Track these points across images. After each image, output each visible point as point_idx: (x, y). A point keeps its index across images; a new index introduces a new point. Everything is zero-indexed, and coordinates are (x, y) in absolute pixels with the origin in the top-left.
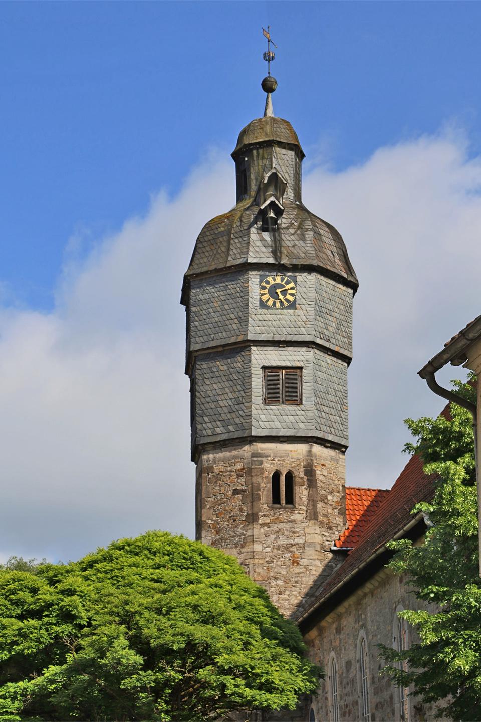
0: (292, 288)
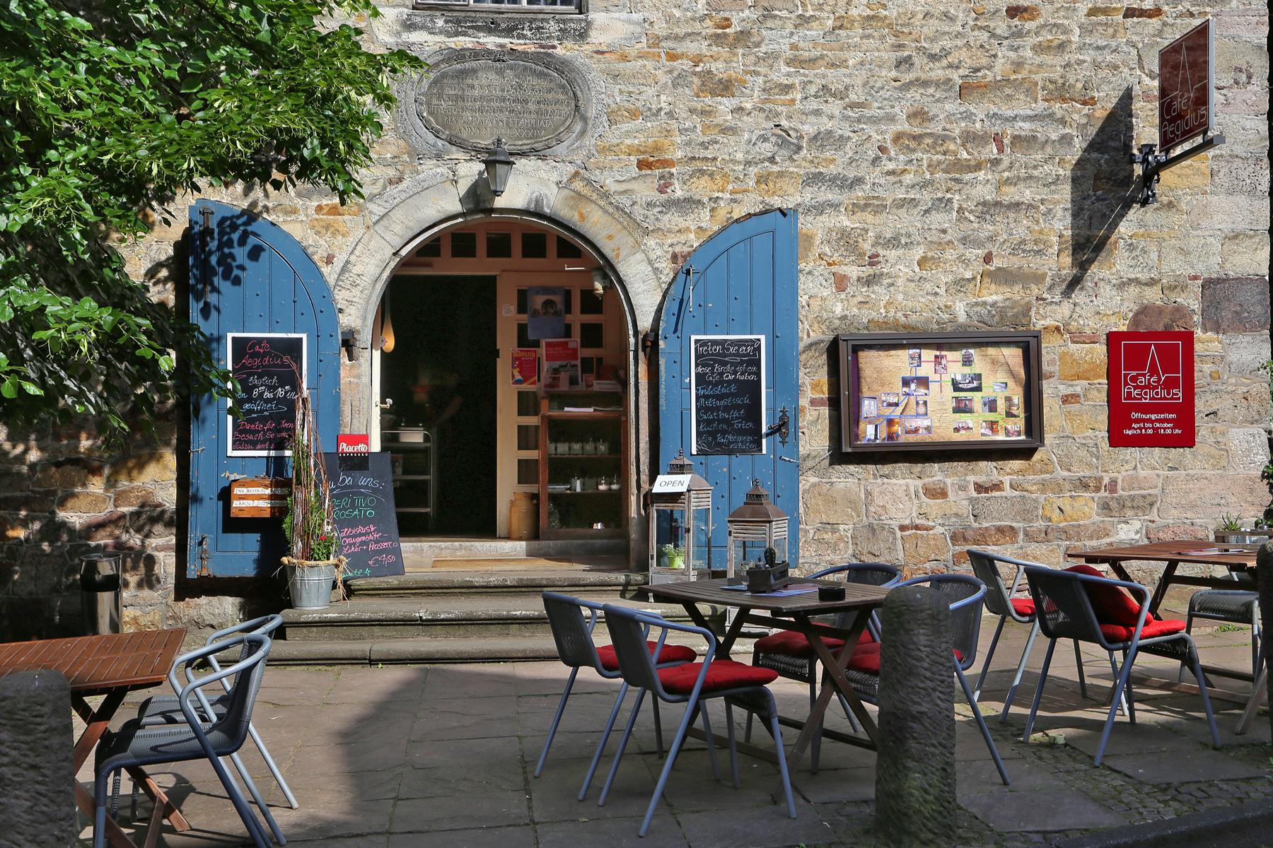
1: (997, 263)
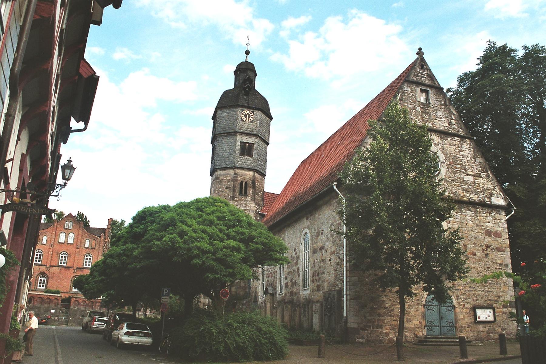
0: (252, 115)
1: (489, 298)
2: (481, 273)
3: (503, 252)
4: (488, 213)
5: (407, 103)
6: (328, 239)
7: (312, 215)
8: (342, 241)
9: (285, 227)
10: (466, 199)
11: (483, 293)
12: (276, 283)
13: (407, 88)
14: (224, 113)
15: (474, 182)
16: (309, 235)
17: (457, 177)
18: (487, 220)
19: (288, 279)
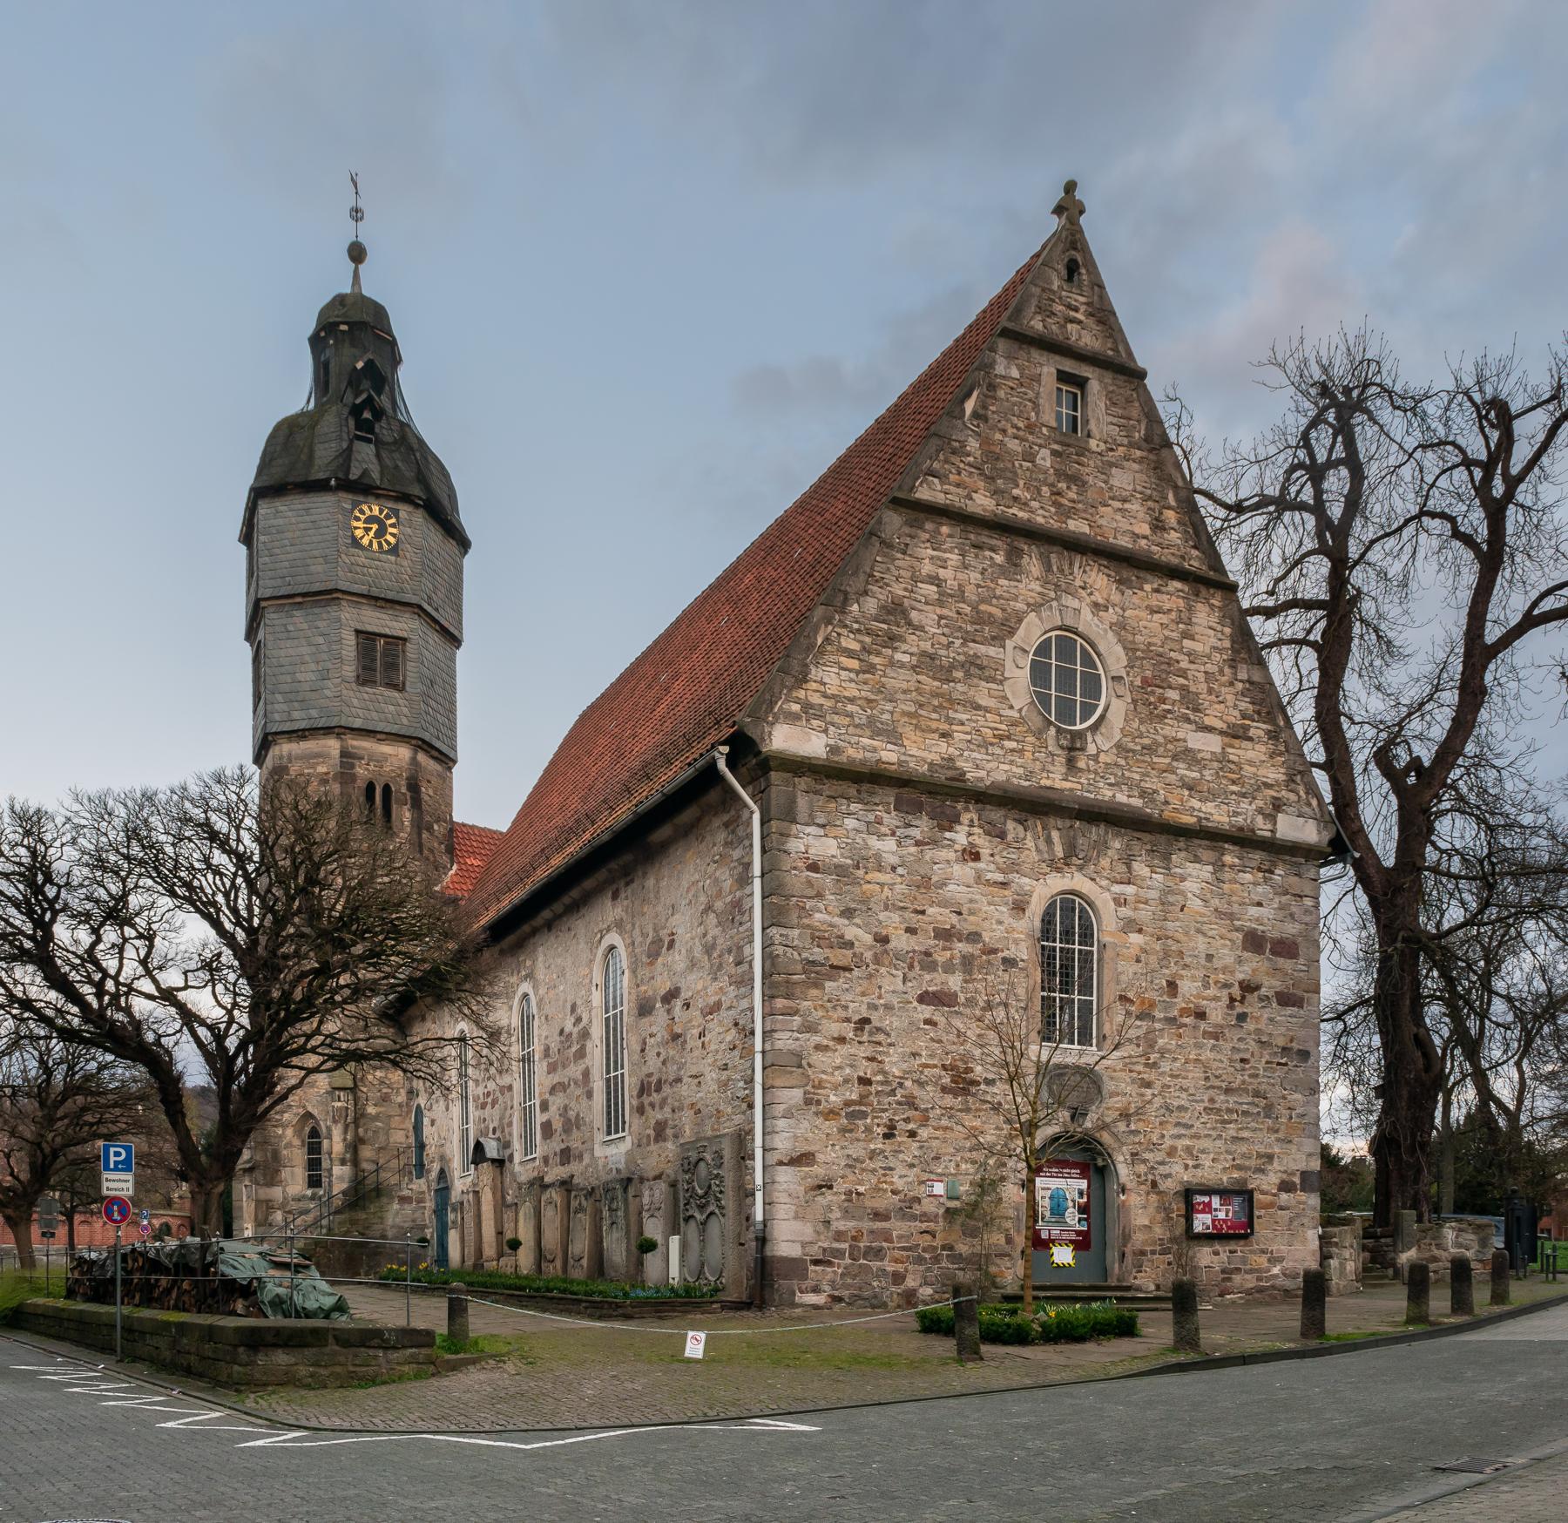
0: (393, 526)
2: (1217, 1077)
3: (1296, 1009)
4: (1259, 870)
5: (1004, 431)
6: (693, 964)
7: (632, 881)
8: (745, 967)
9: (535, 932)
10: (1188, 820)
11: (1219, 1143)
12: (510, 1124)
13: (1005, 368)
14: (281, 514)
15: (1222, 759)
16: (622, 951)
17: (1165, 737)
18: (1252, 896)
19: (553, 1109)
